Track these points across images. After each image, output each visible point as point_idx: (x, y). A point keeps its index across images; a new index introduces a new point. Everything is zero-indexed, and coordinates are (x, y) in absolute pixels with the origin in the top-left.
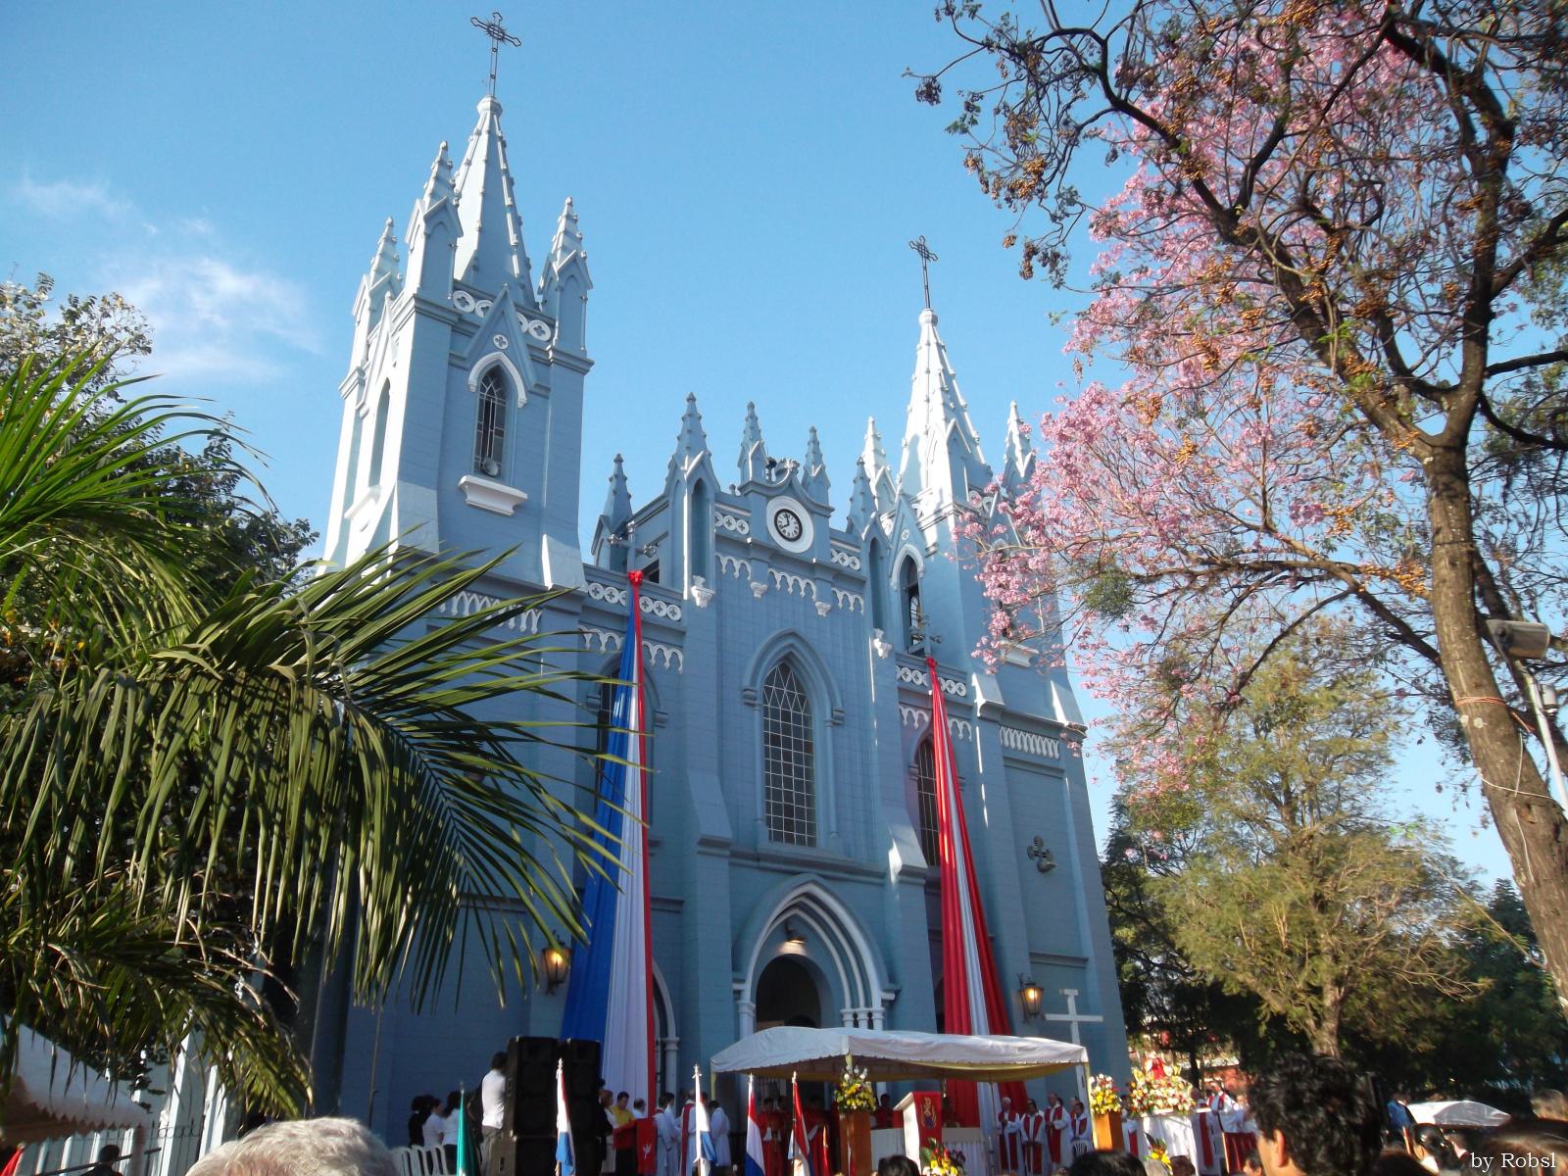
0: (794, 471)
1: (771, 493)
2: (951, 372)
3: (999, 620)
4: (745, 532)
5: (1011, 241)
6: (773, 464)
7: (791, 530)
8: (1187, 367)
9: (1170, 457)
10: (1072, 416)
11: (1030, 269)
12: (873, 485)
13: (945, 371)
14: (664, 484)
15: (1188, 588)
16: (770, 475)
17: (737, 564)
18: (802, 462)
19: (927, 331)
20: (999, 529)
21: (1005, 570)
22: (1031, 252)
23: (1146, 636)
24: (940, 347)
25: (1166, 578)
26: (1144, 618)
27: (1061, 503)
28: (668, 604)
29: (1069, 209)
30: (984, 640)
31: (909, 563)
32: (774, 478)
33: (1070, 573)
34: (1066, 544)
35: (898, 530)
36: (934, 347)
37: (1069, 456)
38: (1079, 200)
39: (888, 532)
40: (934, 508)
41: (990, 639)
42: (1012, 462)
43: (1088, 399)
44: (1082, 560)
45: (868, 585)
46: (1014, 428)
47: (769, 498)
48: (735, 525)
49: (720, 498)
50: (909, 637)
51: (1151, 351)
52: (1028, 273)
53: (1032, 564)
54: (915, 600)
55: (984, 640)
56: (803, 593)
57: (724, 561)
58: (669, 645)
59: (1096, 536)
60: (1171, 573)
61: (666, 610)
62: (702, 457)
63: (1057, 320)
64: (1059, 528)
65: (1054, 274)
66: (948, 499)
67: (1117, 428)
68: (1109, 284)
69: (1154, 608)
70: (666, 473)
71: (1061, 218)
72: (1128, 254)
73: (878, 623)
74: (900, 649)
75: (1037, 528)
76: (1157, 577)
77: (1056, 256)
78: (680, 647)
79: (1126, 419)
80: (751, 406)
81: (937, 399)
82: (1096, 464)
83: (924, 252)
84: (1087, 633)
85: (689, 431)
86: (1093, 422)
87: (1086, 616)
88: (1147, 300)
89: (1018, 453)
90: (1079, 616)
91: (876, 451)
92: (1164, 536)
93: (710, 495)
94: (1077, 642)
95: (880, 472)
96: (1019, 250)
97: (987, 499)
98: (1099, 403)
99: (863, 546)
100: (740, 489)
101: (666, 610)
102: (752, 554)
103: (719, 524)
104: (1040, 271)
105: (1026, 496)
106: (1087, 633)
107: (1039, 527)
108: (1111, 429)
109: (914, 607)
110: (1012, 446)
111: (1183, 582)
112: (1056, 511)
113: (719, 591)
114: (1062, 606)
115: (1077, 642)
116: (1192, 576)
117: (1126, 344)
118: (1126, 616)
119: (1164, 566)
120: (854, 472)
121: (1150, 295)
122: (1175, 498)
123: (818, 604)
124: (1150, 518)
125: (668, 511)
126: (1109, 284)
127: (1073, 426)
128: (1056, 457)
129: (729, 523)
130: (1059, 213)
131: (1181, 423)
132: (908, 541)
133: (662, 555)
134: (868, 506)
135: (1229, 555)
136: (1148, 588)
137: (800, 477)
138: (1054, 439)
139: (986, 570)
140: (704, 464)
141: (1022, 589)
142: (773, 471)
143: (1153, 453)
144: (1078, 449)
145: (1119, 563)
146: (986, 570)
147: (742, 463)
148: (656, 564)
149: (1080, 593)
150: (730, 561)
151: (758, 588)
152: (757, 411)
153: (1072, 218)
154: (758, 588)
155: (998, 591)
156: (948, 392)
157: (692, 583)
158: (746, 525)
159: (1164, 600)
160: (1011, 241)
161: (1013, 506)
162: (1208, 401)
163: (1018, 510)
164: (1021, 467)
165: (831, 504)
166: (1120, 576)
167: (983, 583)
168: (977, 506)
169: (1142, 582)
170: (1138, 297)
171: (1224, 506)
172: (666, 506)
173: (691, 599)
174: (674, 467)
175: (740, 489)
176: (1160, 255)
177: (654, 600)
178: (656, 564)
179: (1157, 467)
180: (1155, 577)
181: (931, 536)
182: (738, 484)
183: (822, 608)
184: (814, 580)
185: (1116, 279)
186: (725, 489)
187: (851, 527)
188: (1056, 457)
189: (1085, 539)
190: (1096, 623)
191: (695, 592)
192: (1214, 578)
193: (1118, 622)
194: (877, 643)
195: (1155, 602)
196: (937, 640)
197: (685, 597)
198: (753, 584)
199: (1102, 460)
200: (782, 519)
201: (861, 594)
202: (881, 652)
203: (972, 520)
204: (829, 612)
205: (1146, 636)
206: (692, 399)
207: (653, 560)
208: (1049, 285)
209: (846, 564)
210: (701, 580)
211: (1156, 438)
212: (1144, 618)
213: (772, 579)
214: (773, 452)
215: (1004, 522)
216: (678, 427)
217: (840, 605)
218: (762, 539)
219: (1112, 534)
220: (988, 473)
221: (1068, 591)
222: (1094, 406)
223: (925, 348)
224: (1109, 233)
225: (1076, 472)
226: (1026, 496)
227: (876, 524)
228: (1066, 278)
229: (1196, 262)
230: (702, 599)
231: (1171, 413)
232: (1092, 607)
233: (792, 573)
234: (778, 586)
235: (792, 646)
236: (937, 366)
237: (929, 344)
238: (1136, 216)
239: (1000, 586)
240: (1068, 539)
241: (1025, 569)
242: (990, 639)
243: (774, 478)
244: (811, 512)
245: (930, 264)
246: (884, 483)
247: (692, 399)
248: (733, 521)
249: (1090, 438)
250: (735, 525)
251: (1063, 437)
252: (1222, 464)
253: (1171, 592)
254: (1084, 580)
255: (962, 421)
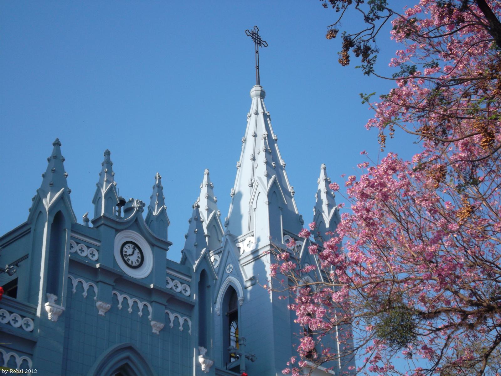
0: (140, 210)
1: (119, 227)
2: (274, 137)
3: (306, 343)
4: (95, 258)
5: (333, 33)
6: (122, 202)
7: (134, 259)
8: (465, 145)
9: (451, 216)
10: (372, 179)
11: (347, 57)
12: (205, 226)
13: (269, 136)
14: (28, 213)
15: (460, 324)
16: (119, 212)
17: (86, 286)
18: (148, 203)
19: (256, 104)
20: (308, 267)
21: (312, 302)
22: (348, 43)
23: (425, 363)
24: (266, 116)
25: (443, 316)
26: (425, 348)
27: (361, 249)
28: (23, 317)
29: (380, 13)
30: (293, 360)
31: (231, 292)
32: (123, 215)
33: (366, 307)
34: (364, 283)
35: (223, 264)
36: (261, 116)
37: (368, 211)
38: (387, 6)
39: (216, 266)
40: (252, 247)
41: (298, 359)
42: (319, 213)
43: (385, 166)
44: (375, 297)
45: (196, 310)
46: (322, 186)
47: (118, 231)
48: (86, 252)
49: (75, 228)
50: (228, 355)
51: (439, 129)
52: (346, 61)
53: (335, 298)
54: (234, 324)
55: (293, 360)
56: (140, 313)
57: (75, 282)
58: (21, 353)
59: (388, 277)
60: (447, 311)
61: (21, 322)
62: (63, 193)
63: (367, 99)
64: (358, 269)
65: (366, 63)
66: (266, 240)
67: (408, 191)
68: (407, 74)
69: (432, 341)
70: (30, 204)
71: (372, 20)
72: (422, 53)
73: (202, 342)
74: (220, 365)
75: (340, 268)
76: (436, 314)
77: (367, 49)
78: (31, 355)
79: (414, 184)
80: (108, 153)
81: (262, 158)
82: (390, 219)
83: (258, 41)
84: (378, 358)
85: (53, 171)
86: (389, 185)
87: (377, 343)
88: (437, 89)
89: (325, 208)
90: (372, 343)
91: (209, 198)
92: (442, 282)
93: (67, 225)
94: (369, 365)
95: (211, 215)
96: (339, 41)
97: (298, 243)
98: (394, 170)
99: (194, 276)
100: (94, 222)
101: (21, 322)
102: (100, 278)
103: (73, 251)
104: (356, 60)
105: (332, 241)
106: (378, 358)
107: (341, 267)
108: (402, 191)
109: (233, 330)
110: (320, 202)
111: (457, 319)
112: (356, 255)
113: (69, 307)
114: (356, 334)
115: (369, 365)
116: (464, 315)
117: (418, 125)
118: (410, 345)
119: (441, 305)
120: (190, 215)
121: (439, 85)
122: (453, 251)
123: (153, 323)
124: (431, 265)
125: (29, 260)
126: (407, 74)
127: (373, 186)
128: (357, 211)
129: (82, 251)
130: (371, 16)
131: (460, 188)
132: (231, 274)
133: (21, 274)
134: (200, 243)
135: (493, 299)
136: (428, 322)
137: (144, 215)
138: (356, 196)
139: (297, 301)
140: (64, 199)
141: (326, 318)
142: (122, 208)
143: (436, 212)
144: (375, 206)
145: (405, 301)
146: (297, 301)
147: (96, 200)
148: (15, 282)
149: (373, 324)
150: (80, 282)
151: (102, 307)
152: (112, 158)
153: (382, 20)
154: (102, 307)
155: (305, 318)
156: (270, 153)
157: (45, 300)
158: (96, 253)
159: (441, 334)
160: (333, 33)
161: (320, 249)
162: (480, 173)
163: (325, 252)
164: (327, 218)
165: (169, 239)
166: (406, 311)
167: (294, 312)
168: (290, 246)
169: (424, 318)
170: (429, 87)
171: (491, 259)
172: (28, 232)
173: (44, 312)
174: (38, 201)
175: (94, 222)
176: (446, 55)
177: (11, 313)
178: (15, 282)
179: (438, 224)
180: (435, 314)
181: (248, 271)
182: (91, 217)
183: (156, 327)
184: (151, 302)
185: (412, 70)
186: (80, 221)
187: (185, 260)
188: (357, 211)
189: (378, 280)
190: (384, 350)
191: (47, 308)
192: (481, 318)
193: (403, 351)
194: (201, 360)
195: (433, 335)
196: (250, 358)
197: (38, 314)
198: (99, 303)
199: (395, 215)
200: (128, 250)
201: (190, 317)
202: (203, 367)
203: (287, 259)
204: (162, 330)
205: (425, 363)
206: (57, 144)
207: (13, 278)
208: (361, 71)
209: (178, 290)
210: (53, 297)
211: (438, 201)
212: (425, 348)
213: (115, 300)
214: (123, 193)
215: (312, 263)
216: (44, 166)
217: (172, 325)
218: (110, 266)
219: (401, 276)
220: (300, 221)
221: (363, 322)
222: (390, 172)
223: (254, 116)
224: (408, 35)
225: (373, 224)
226: (332, 241)
227: (206, 258)
228: (375, 67)
229: (473, 64)
230: (53, 313)
231: (452, 181)
232: (382, 336)
233: (132, 296)
234: (120, 306)
235: (128, 358)
236: (263, 131)
237: (257, 113)
238: (429, 24)
239: (309, 315)
240: (365, 279)
241: (328, 302)
242: (298, 359)
243: (123, 215)
244: (152, 245)
245: (261, 49)
246: (214, 224)
247: (57, 144)
248: (85, 248)
249: (386, 197)
250: (86, 252)
251: (364, 196)
252: (490, 225)
253: (446, 327)
254: (376, 314)
255: (280, 177)
